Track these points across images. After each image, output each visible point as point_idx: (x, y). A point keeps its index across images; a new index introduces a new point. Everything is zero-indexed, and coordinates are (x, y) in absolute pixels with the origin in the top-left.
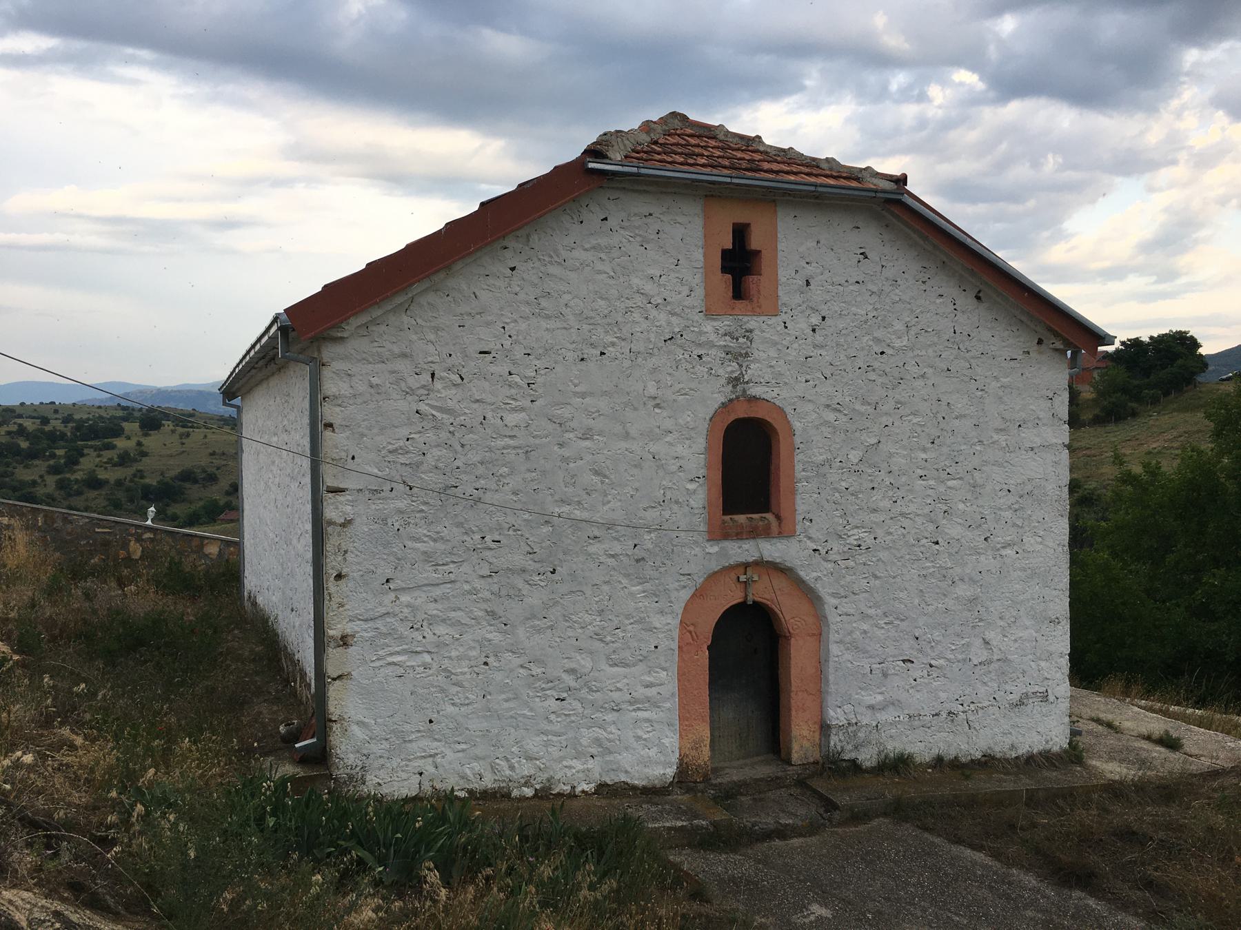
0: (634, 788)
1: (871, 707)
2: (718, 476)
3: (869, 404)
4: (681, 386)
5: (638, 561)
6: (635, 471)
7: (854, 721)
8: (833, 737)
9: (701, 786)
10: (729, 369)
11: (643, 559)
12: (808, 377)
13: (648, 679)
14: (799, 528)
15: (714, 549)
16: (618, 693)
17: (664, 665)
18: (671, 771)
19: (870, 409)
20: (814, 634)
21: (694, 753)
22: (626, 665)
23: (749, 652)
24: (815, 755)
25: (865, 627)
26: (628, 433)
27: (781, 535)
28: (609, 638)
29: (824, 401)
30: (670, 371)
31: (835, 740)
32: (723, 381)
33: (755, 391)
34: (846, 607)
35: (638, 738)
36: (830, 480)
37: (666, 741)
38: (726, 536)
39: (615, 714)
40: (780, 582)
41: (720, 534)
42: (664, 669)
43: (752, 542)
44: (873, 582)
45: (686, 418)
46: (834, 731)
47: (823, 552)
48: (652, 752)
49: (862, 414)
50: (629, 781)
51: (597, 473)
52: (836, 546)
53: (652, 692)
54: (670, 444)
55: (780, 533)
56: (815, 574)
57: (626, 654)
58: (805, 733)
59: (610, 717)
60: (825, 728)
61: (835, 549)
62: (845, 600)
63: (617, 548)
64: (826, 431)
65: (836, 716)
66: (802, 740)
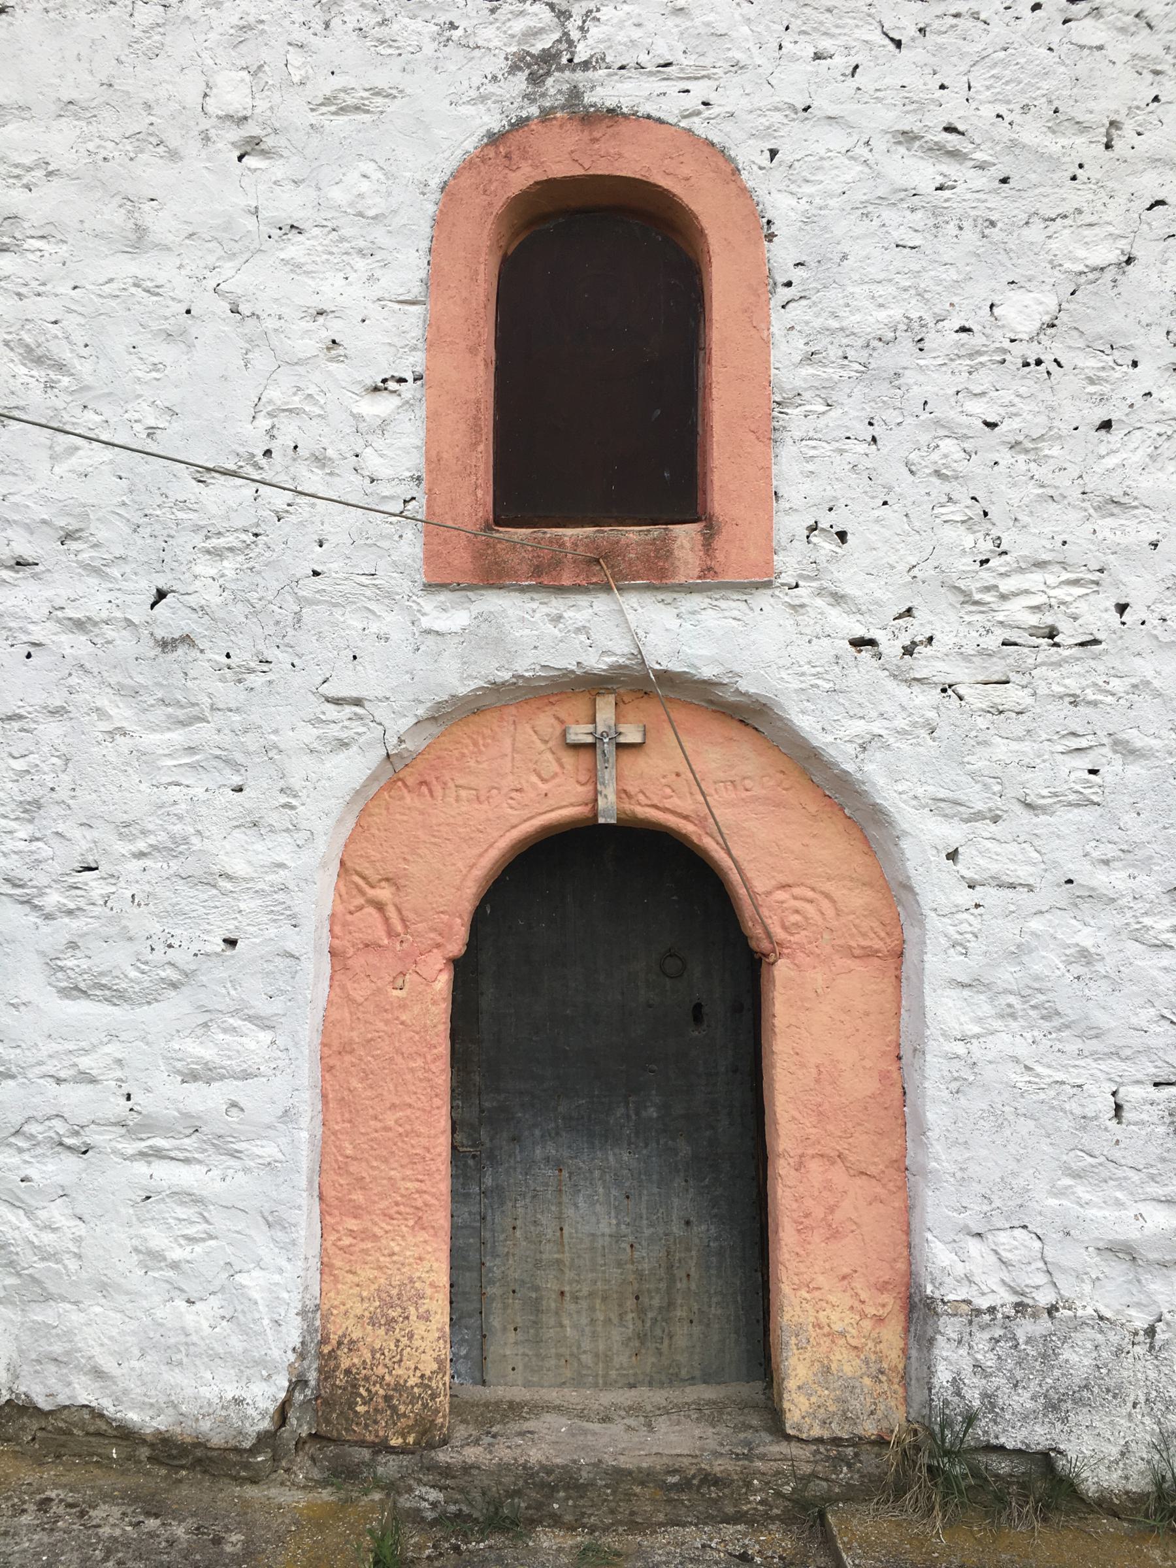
0: (126, 1435)
1: (1124, 1252)
2: (475, 379)
3: (1082, 128)
4: (338, 82)
5: (166, 645)
6: (165, 353)
7: (1044, 1298)
8: (943, 1350)
9: (388, 1467)
10: (518, 26)
11: (187, 639)
12: (825, 44)
13: (199, 1050)
14: (788, 564)
15: (452, 615)
16: (85, 1090)
17: (262, 1006)
18: (263, 1395)
19: (1087, 148)
20: (869, 954)
21: (378, 1337)
22: (117, 997)
23: (613, 990)
24: (883, 1412)
25: (1086, 938)
26: (141, 231)
27: (710, 581)
28: (53, 899)
29: (893, 118)
30: (300, 35)
31: (953, 1362)
32: (498, 65)
33: (607, 92)
34: (989, 853)
35: (152, 1258)
36: (917, 394)
37: (253, 1282)
38: (491, 575)
39: (72, 1161)
40: (719, 756)
41: (472, 568)
42: (263, 1023)
43: (601, 603)
44: (1113, 768)
45: (352, 184)
46: (950, 1327)
47: (891, 647)
48: (199, 1319)
49: (1054, 162)
50: (110, 1410)
51: (35, 357)
52: (942, 622)
53: (206, 1100)
54: (296, 267)
55: (707, 571)
56: (858, 727)
57: (117, 959)
58: (840, 1319)
59: (53, 1170)
60: (918, 1310)
61: (944, 641)
62: (986, 828)
63: (95, 600)
64: (901, 223)
65: (957, 1266)
66: (829, 1350)
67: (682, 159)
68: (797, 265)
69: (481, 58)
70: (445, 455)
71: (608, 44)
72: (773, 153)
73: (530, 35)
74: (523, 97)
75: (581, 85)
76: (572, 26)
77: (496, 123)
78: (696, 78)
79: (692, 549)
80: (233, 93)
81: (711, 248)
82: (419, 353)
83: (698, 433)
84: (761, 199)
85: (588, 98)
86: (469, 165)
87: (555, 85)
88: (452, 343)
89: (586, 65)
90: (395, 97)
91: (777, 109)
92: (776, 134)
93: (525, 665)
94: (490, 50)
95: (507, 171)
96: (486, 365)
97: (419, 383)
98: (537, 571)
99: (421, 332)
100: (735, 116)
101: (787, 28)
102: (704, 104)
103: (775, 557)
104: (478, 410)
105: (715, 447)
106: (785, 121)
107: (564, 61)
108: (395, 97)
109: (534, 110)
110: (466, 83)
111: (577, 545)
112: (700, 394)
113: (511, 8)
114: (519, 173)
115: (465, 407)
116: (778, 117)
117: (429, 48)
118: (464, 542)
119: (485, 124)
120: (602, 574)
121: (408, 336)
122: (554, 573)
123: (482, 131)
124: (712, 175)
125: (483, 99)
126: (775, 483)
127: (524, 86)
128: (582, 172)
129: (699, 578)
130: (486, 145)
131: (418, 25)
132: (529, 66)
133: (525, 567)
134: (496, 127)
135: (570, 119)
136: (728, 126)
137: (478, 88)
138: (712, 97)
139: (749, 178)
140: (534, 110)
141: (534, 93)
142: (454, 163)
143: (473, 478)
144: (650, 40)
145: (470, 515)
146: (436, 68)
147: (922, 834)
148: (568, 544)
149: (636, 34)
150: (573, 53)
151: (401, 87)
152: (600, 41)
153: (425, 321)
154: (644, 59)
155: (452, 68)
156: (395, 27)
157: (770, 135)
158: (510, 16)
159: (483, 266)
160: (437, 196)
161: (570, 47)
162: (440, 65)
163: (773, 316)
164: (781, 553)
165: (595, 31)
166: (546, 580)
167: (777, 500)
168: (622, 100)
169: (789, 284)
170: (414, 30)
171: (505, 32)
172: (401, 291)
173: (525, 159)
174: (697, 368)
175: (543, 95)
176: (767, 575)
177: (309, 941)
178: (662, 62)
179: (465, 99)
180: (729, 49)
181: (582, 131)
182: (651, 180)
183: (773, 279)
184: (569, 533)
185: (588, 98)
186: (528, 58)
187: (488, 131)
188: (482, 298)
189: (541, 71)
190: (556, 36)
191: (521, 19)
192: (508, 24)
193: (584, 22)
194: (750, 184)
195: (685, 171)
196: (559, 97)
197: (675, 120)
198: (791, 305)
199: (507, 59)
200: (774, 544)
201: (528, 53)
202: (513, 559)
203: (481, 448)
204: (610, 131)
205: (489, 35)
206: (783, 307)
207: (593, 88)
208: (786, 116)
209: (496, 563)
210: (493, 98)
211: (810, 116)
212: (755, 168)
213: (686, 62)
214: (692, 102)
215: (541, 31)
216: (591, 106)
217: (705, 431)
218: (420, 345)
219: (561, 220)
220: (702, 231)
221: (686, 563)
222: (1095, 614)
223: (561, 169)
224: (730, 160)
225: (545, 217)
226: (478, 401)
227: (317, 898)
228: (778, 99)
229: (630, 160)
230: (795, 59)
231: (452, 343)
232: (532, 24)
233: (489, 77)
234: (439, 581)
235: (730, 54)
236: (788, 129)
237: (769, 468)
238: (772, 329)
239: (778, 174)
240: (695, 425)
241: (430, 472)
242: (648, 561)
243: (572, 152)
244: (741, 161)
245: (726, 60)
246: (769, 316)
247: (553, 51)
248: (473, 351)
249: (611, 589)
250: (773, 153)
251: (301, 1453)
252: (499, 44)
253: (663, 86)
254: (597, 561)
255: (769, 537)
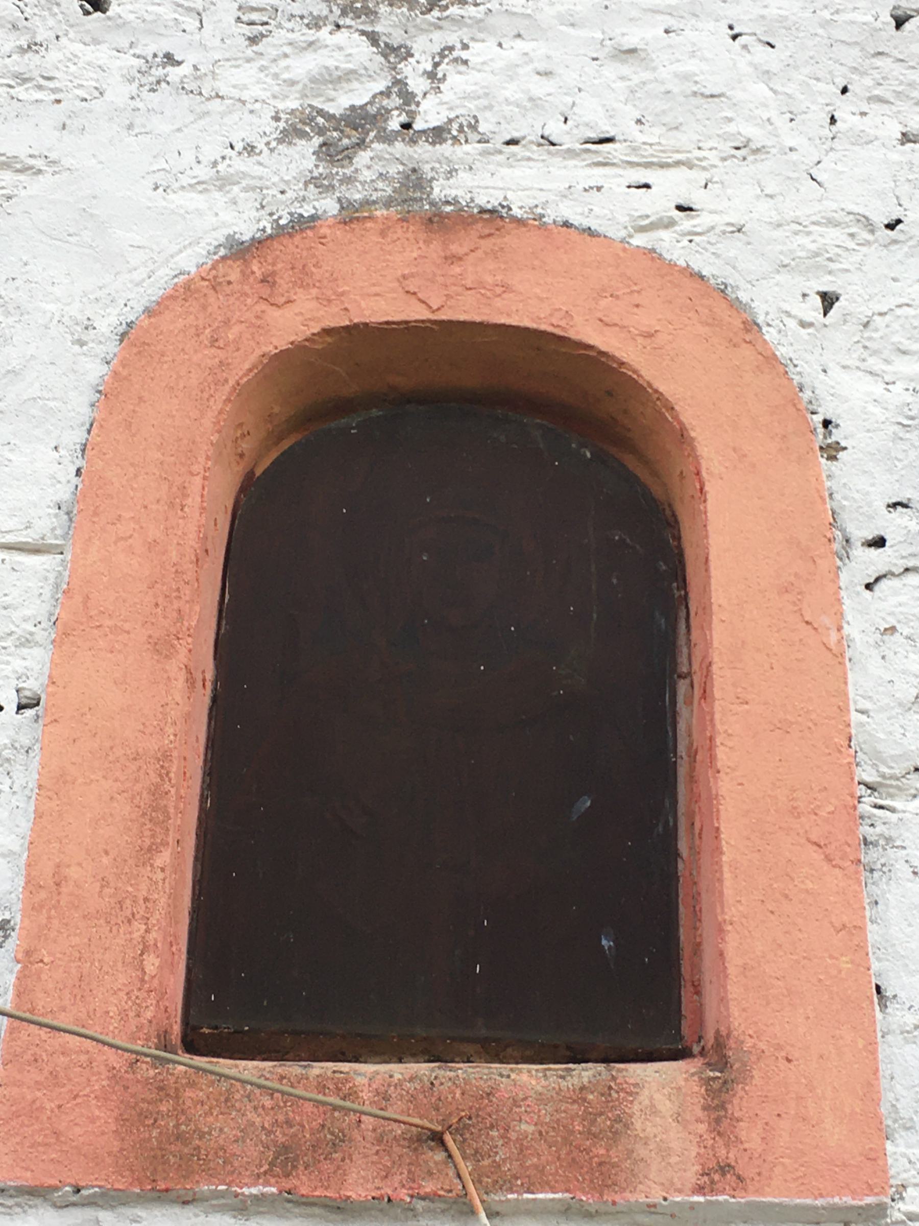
10: (304, 66)
67: (636, 299)
68: (895, 505)
69: (223, 115)
70: (74, 873)
71: (485, 102)
72: (828, 300)
73: (325, 82)
74: (306, 184)
75: (426, 168)
76: (414, 75)
77: (247, 225)
78: (663, 166)
79: (678, 1118)
81: (704, 464)
82: (37, 652)
83: (677, 855)
84: (806, 380)
85: (439, 190)
86: (185, 292)
87: (374, 167)
88: (115, 629)
89: (438, 134)
90: (40, 172)
91: (832, 223)
92: (832, 266)
94: (244, 103)
95: (263, 306)
96: (191, 681)
97: (29, 713)
98: (284, 1160)
99: (46, 607)
101: (844, 90)
102: (680, 208)
103: (889, 1146)
104: (164, 775)
105: (727, 875)
106: (851, 244)
107: (394, 124)
108: (40, 172)
109: (329, 206)
110: (189, 157)
111: (387, 1098)
112: (682, 771)
113: (290, 36)
114: (288, 312)
115: (133, 767)
116: (835, 236)
117: (118, 93)
118: (101, 1083)
119: (224, 224)
121: (16, 615)
122: (326, 1166)
123: (220, 237)
124: (703, 330)
125: (223, 182)
126: (875, 966)
127: (310, 162)
128: (425, 315)
129: (700, 1189)
130: (224, 258)
131: (102, 55)
132: (321, 131)
133: (252, 1150)
134: (247, 231)
135: (402, 220)
136: (733, 248)
137: (215, 164)
138: (696, 198)
139: (784, 341)
140: (329, 206)
141: (330, 176)
142: (154, 291)
143: (139, 928)
144: (569, 100)
145: (123, 1015)
146: (130, 127)
148: (365, 1095)
149: (540, 87)
150: (412, 115)
151: (53, 156)
152: (467, 97)
153: (57, 586)
154: (555, 129)
155: (166, 128)
156: (54, 56)
157: (818, 267)
158: (287, 49)
159: (198, 480)
160: (112, 347)
161: (407, 103)
162: (137, 122)
163: (848, 605)
164: (902, 1138)
165: (456, 81)
166: (304, 1184)
167: (883, 1006)
168: (510, 195)
169: (879, 542)
170: (90, 55)
171: (276, 76)
172: (11, 524)
173: (304, 286)
174: (674, 714)
175: (348, 180)
176: (870, 1189)
178: (594, 135)
179: (185, 180)
180: (730, 120)
181: (427, 242)
182: (572, 334)
183: (843, 531)
184: (365, 1074)
185: (439, 190)
186: (320, 120)
187: (229, 237)
188: (192, 541)
189: (346, 141)
190: (380, 85)
191: (309, 56)
192: (283, 63)
193: (436, 65)
194: (782, 352)
195: (645, 320)
196: (380, 185)
197: (623, 233)
198: (884, 584)
199: (277, 119)
200: (884, 1109)
201: (321, 112)
202: (222, 1128)
203: (164, 858)
204: (486, 244)
205: (245, 78)
206: (868, 587)
207: (451, 173)
208: (852, 235)
209: (178, 1137)
210: (244, 183)
211: (902, 237)
212: (792, 324)
213: (641, 138)
214: (657, 203)
215: (349, 76)
216: (448, 203)
217: (695, 852)
218: (41, 635)
219: (375, 412)
220: (682, 436)
221: (664, 1151)
224: (736, 305)
225: (343, 407)
226: (166, 756)
228: (835, 206)
229: (529, 300)
230: (863, 140)
231: (115, 629)
232: (331, 63)
233: (239, 146)
234: (27, 1179)
235: (732, 128)
236: (857, 258)
237: (862, 929)
238: (847, 630)
239: (839, 330)
240: (672, 835)
241: (32, 908)
242: (566, 1141)
243: (404, 277)
244: (762, 310)
245: (725, 137)
246: (839, 601)
247: (372, 110)
248: (162, 648)
249: (473, 1212)
250: (828, 300)
252: (264, 95)
253: (597, 175)
254: (437, 1139)
255: (870, 1091)
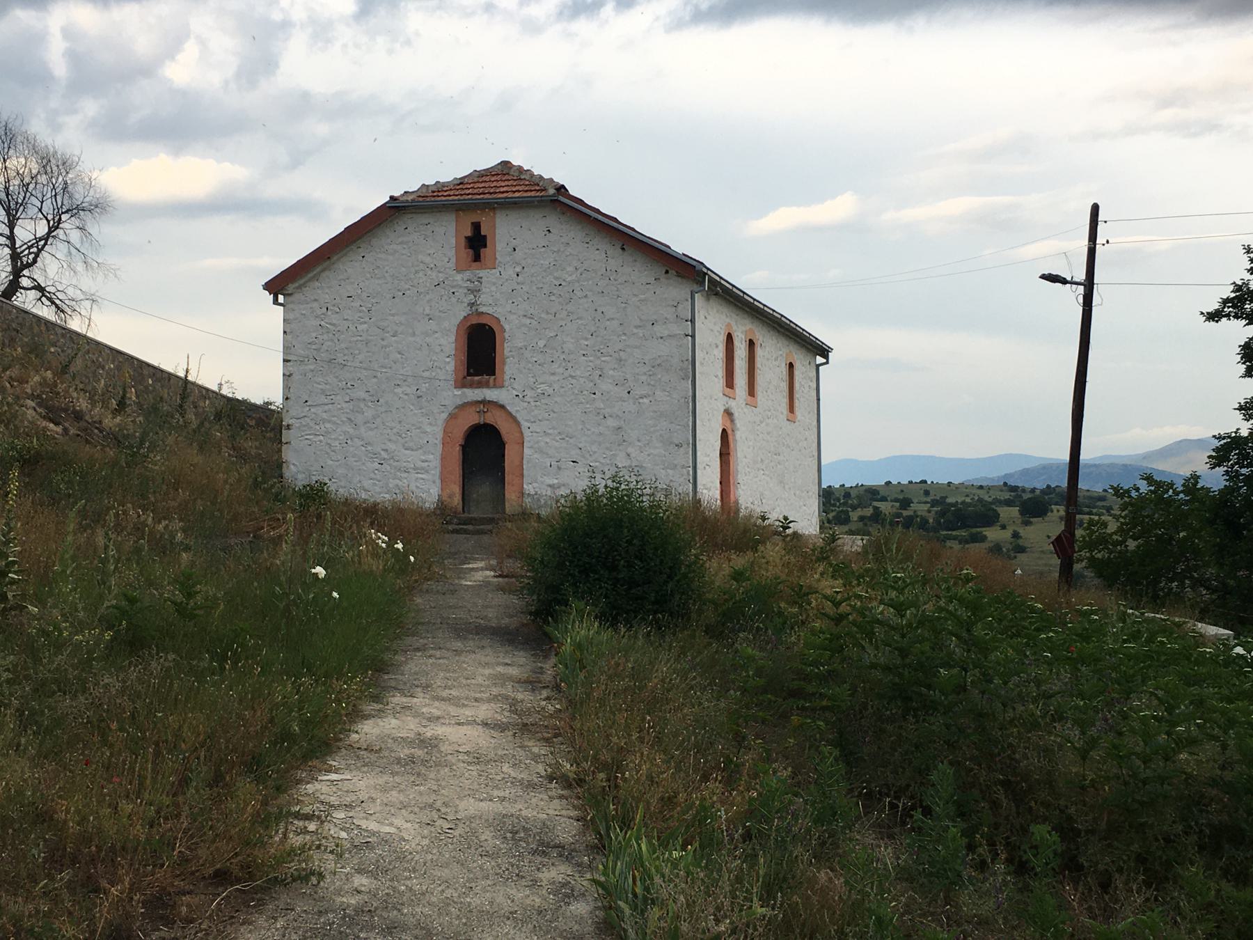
14: (506, 384)
19: (551, 317)
27: (495, 386)
29: (522, 313)
34: (534, 427)
38: (463, 386)
41: (461, 384)
45: (446, 324)
57: (411, 444)
63: (408, 390)
65: (529, 488)
80: (427, 311)
93: (469, 399)
100: (498, 312)
120: (480, 385)
147: (525, 424)
177: (439, 442)
222: (551, 391)
223: (474, 322)
227: (440, 435)
251: (277, 16)
